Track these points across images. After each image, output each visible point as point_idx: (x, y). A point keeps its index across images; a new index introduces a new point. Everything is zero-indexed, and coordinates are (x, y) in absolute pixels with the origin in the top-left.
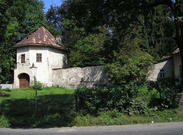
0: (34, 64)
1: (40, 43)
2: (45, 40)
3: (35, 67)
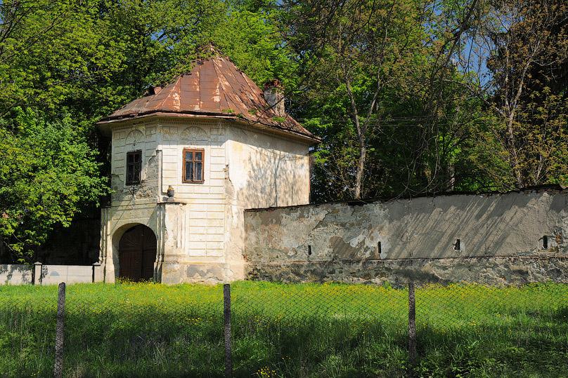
0: (174, 188)
1: (197, 109)
2: (217, 99)
3: (176, 200)
